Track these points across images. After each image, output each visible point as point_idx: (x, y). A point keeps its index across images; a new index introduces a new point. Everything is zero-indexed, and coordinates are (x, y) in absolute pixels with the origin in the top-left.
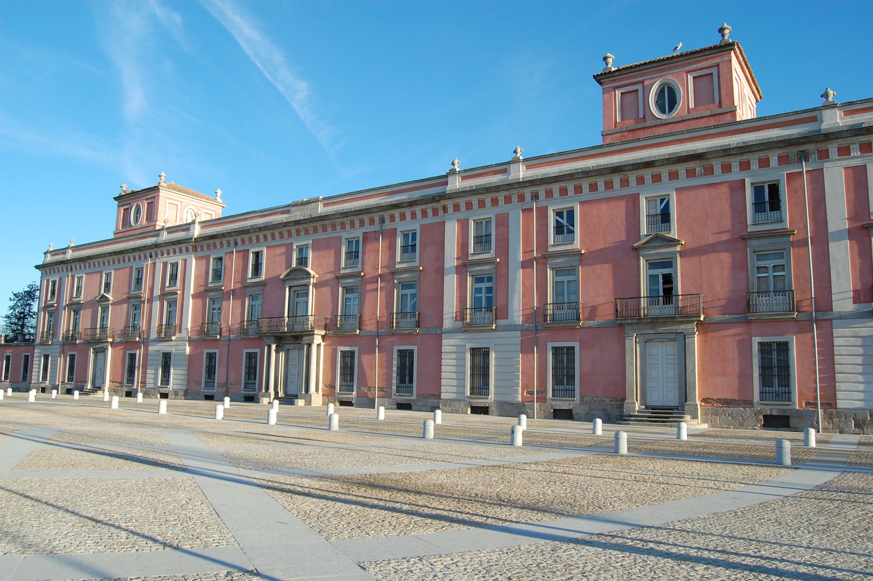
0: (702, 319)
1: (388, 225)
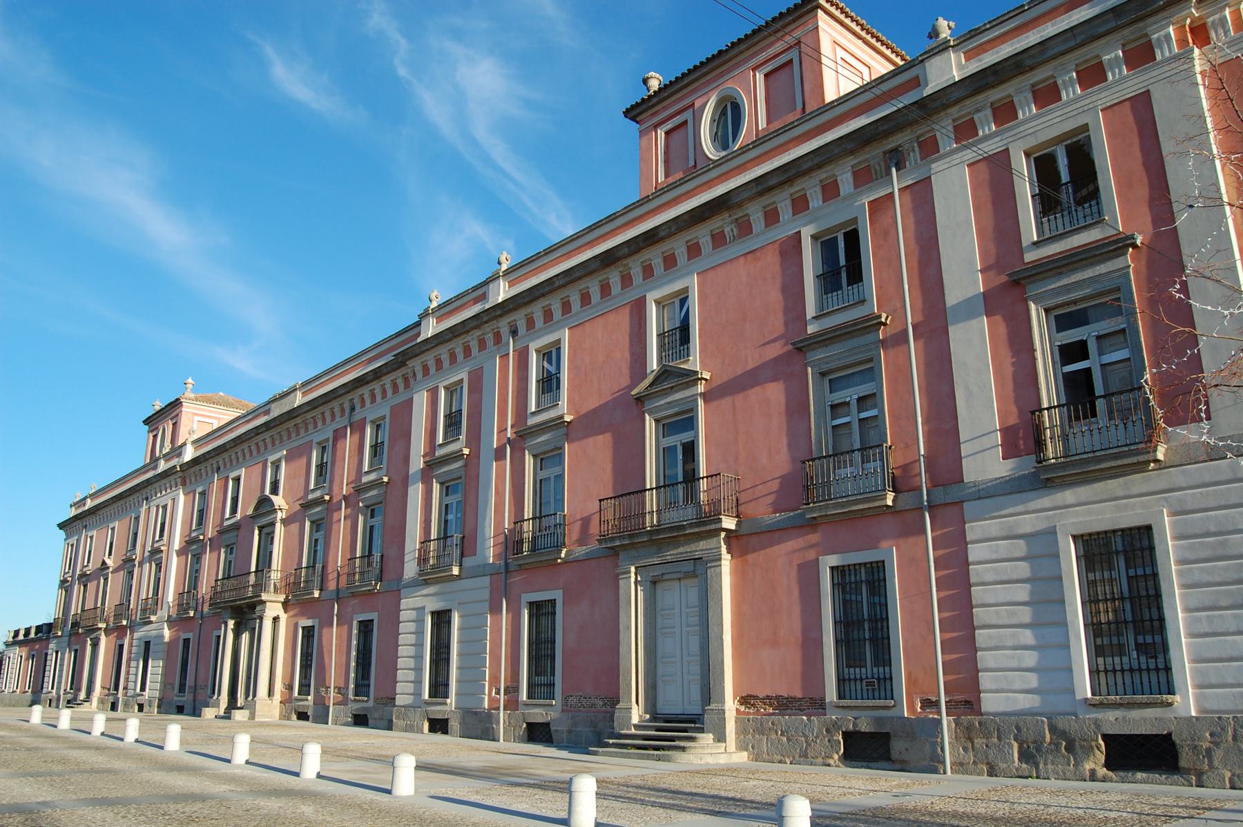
0: (890, 503)
1: (357, 416)
